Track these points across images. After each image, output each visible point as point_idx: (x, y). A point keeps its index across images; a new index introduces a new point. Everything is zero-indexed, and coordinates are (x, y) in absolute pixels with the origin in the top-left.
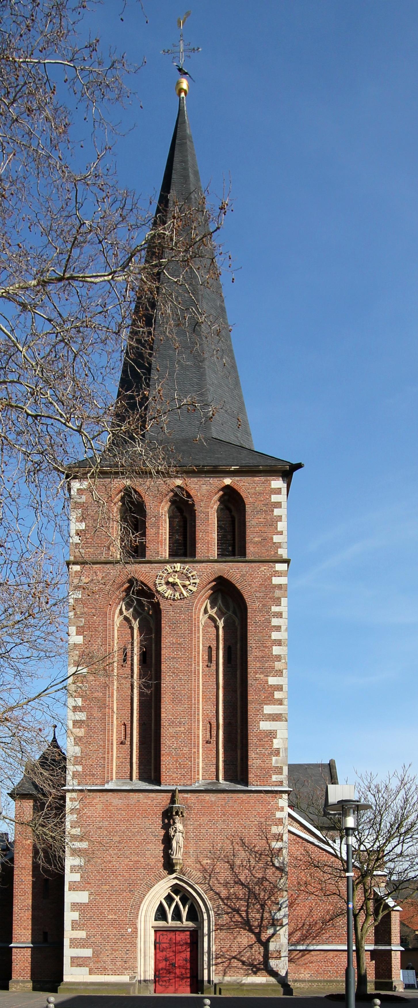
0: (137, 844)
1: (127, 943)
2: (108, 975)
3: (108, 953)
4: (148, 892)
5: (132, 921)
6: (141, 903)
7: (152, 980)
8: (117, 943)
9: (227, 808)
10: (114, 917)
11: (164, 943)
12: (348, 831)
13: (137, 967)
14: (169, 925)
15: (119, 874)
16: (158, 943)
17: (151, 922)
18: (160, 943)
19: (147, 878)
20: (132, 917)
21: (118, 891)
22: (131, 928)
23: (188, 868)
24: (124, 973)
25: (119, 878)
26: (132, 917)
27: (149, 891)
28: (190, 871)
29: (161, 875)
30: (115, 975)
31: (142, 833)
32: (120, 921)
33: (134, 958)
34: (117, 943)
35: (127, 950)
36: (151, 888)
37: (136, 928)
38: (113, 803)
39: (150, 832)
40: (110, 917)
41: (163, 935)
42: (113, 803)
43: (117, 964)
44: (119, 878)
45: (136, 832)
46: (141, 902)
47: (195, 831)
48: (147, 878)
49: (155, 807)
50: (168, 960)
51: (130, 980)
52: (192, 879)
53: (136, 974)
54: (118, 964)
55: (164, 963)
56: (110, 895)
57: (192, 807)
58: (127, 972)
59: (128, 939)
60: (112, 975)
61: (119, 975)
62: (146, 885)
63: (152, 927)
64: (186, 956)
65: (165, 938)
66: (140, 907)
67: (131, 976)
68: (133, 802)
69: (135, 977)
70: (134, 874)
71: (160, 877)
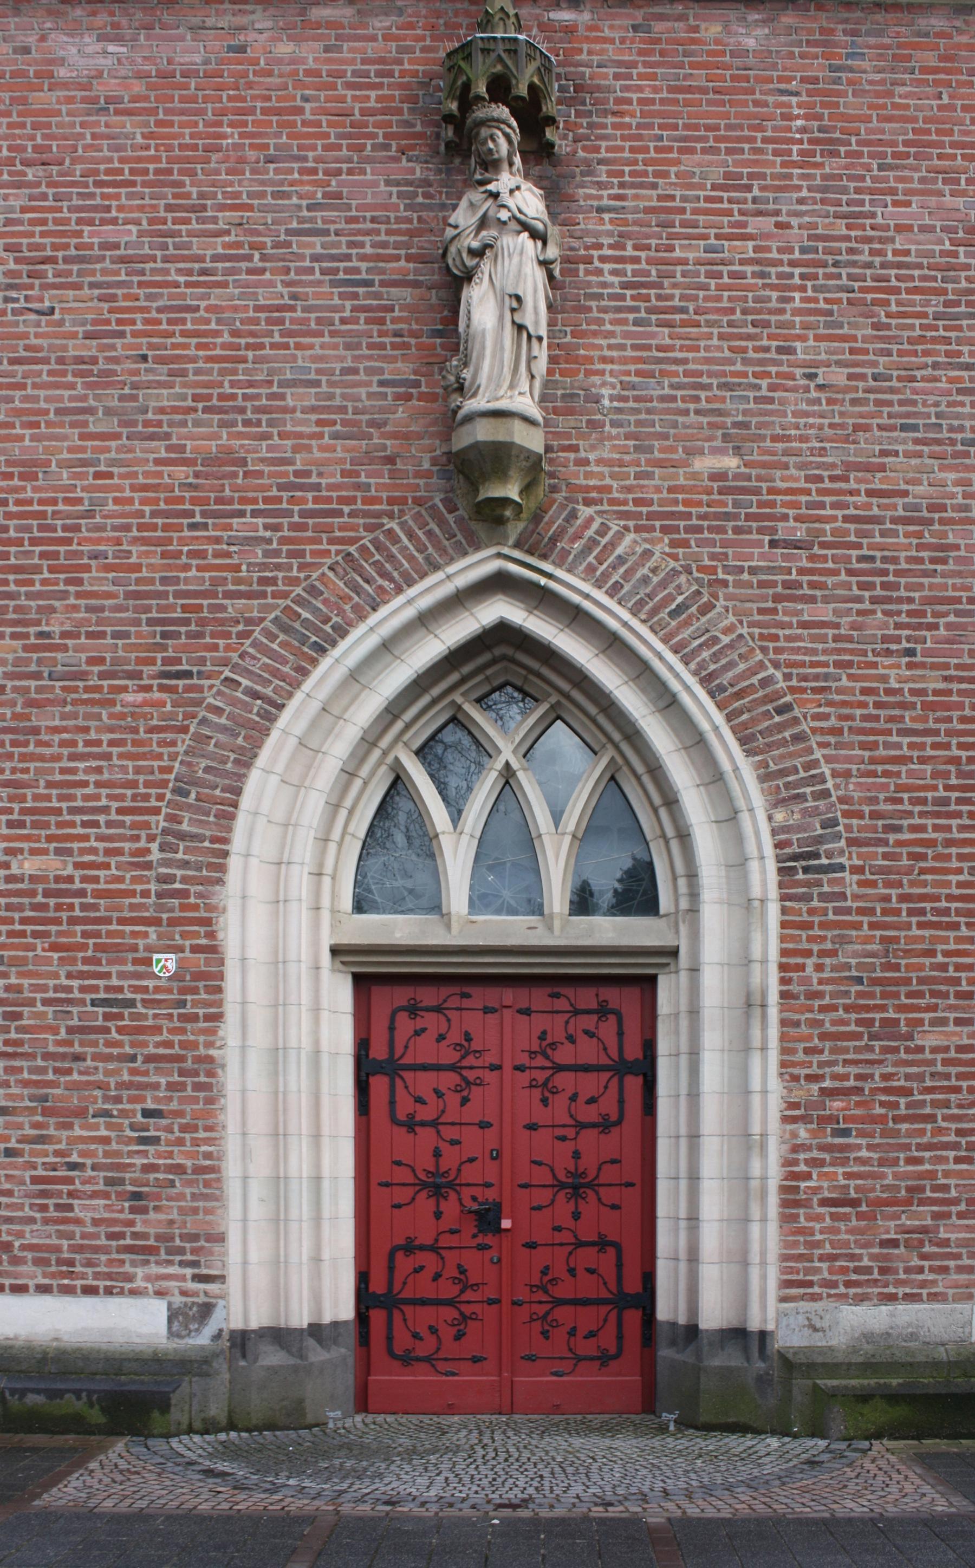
0: (226, 338)
1: (149, 1059)
2: (19, 1289)
3: (15, 1134)
4: (297, 685)
5: (184, 894)
6: (248, 765)
7: (335, 1324)
8: (78, 1058)
9: (849, 103)
10: (51, 865)
11: (425, 1068)
12: (186, 1327)
13: (221, 1238)
14: (455, 938)
15: (95, 556)
16: (380, 1068)
17: (326, 915)
18: (621, 1068)
19: (295, 581)
20: (185, 864)
21: (82, 676)
22: (179, 949)
23: (585, 512)
24: (130, 1278)
25: (96, 581)
26: (185, 864)
27: (304, 673)
28: (603, 531)
29: (391, 558)
30: (68, 1291)
31: (257, 262)
32: (98, 894)
33: (198, 1170)
34: (78, 1058)
35: (147, 1113)
36: (323, 651)
37: (213, 949)
38: (62, 62)
39: (316, 258)
40: (28, 866)
41: (413, 1010)
42: (62, 62)
43: (78, 1213)
44: (96, 581)
45: (216, 258)
46: (246, 760)
47: (630, 252)
48: (295, 581)
49: (349, 86)
50: (451, 1185)
51: (171, 1334)
52: (617, 587)
53: (212, 1287)
54: (87, 1216)
55: (425, 1204)
56: (31, 703)
57: (609, 90)
58: (155, 1269)
59: (157, 1030)
60: (44, 1289)
61: (90, 1291)
62: (286, 629)
63: (336, 951)
64: (577, 1155)
65: (431, 1035)
66: (238, 792)
67: (178, 1300)
68: (198, 58)
69: (206, 1310)
70: (201, 554)
71: (384, 575)
